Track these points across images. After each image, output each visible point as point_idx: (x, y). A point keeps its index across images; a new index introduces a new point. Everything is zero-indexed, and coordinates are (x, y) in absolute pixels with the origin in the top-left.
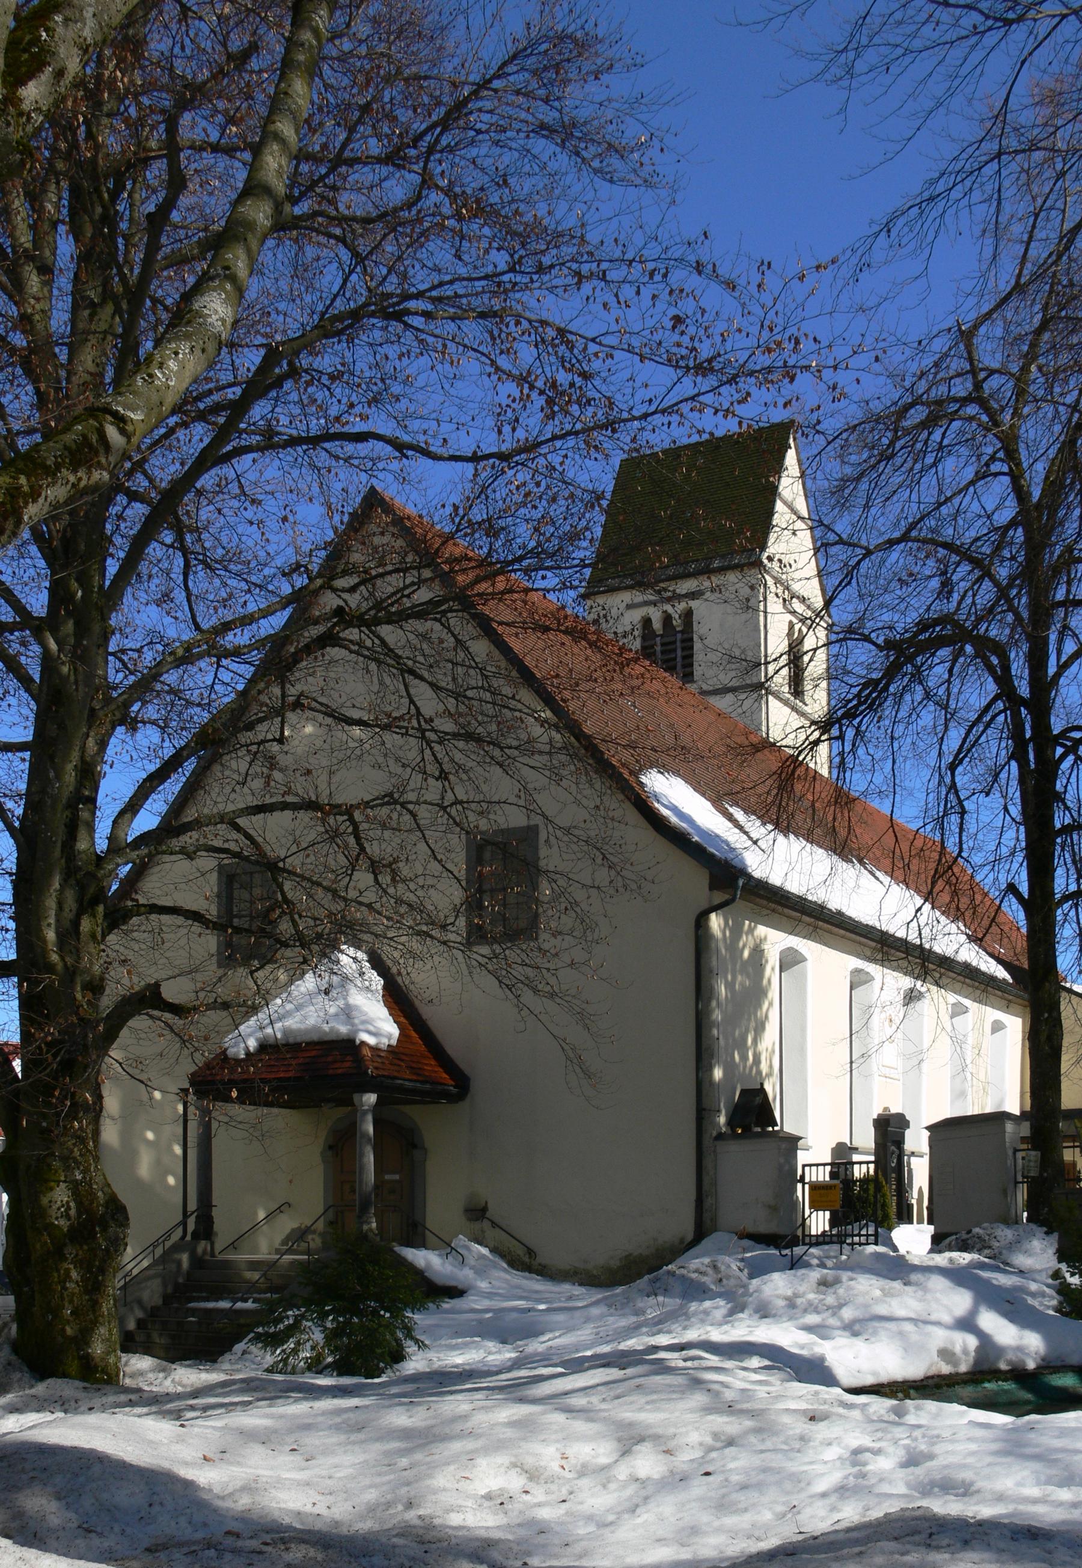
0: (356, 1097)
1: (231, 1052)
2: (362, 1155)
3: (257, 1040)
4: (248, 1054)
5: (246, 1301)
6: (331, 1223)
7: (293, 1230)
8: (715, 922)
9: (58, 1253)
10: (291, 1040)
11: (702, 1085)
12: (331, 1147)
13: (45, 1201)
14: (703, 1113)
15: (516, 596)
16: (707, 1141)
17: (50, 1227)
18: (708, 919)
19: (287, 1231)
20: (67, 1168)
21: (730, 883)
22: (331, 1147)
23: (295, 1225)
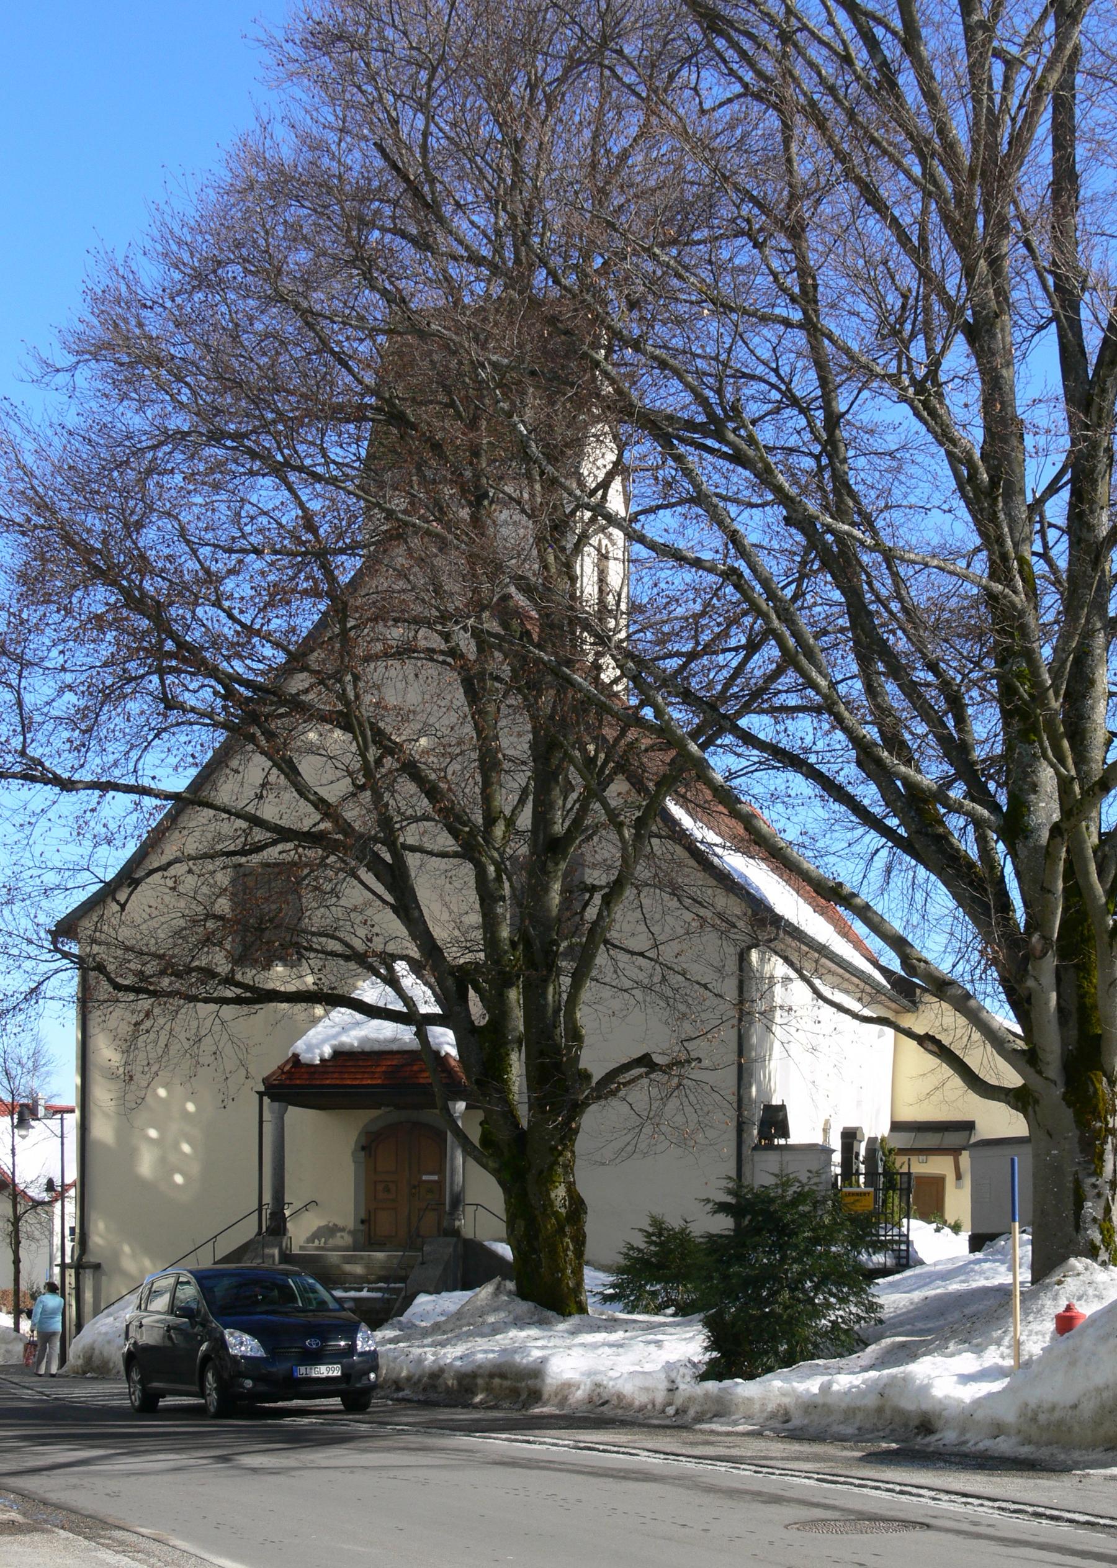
0: (450, 1104)
1: (305, 1057)
2: (453, 1159)
3: (333, 1047)
4: (322, 1060)
5: (360, 1290)
6: (363, 1222)
7: (319, 1228)
8: (754, 955)
9: (561, 1231)
10: (367, 1049)
11: (741, 1102)
12: (363, 1148)
13: (553, 1195)
14: (741, 1128)
15: (150, 443)
16: (747, 1151)
17: (556, 1214)
18: (749, 955)
19: (315, 1228)
20: (566, 1173)
21: (765, 924)
22: (363, 1148)
23: (323, 1223)
